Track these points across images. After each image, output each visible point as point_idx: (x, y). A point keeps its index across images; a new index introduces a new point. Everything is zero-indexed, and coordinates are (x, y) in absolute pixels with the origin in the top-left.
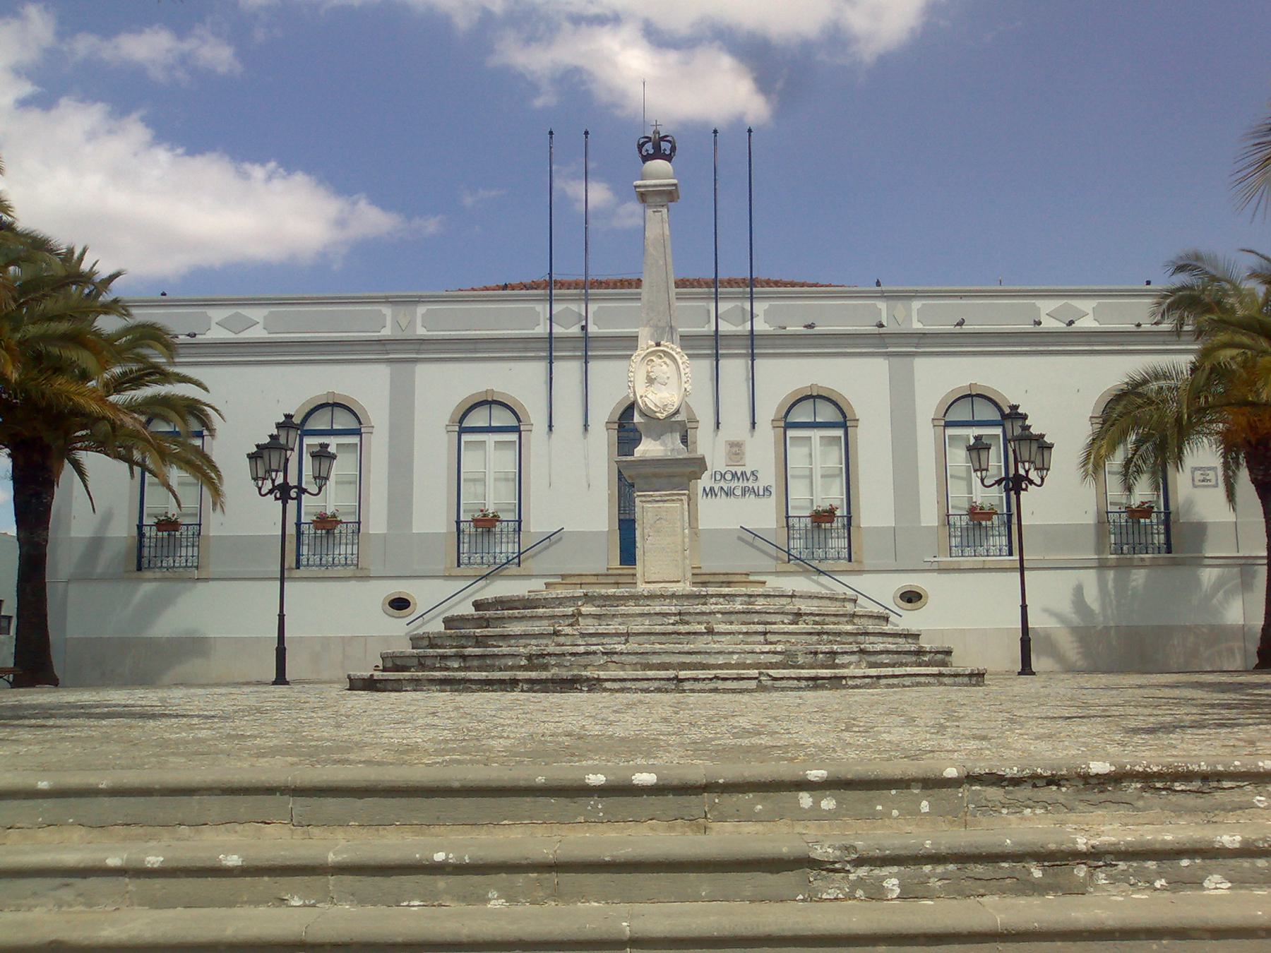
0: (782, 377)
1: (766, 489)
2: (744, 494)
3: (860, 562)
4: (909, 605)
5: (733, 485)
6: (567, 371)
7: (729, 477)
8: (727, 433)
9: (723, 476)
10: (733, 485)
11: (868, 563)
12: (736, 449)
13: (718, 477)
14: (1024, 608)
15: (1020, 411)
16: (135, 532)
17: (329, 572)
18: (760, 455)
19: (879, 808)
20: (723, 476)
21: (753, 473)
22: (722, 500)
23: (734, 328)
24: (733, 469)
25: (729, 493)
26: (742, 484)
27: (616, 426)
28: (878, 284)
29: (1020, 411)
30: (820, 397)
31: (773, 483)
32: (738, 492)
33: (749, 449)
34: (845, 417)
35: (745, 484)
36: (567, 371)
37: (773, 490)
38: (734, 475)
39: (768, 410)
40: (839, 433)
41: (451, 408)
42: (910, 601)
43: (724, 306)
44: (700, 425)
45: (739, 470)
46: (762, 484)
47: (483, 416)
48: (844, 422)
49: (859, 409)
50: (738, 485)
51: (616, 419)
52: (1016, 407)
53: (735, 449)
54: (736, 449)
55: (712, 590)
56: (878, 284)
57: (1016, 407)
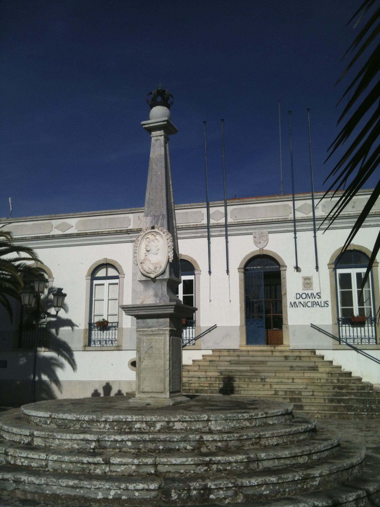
1: (326, 303)
2: (313, 306)
5: (306, 300)
6: (218, 242)
7: (304, 296)
9: (301, 296)
10: (306, 300)
12: (307, 282)
13: (298, 296)
14: (326, 161)
17: (104, 346)
20: (301, 296)
21: (317, 294)
23: (305, 216)
24: (306, 292)
25: (305, 305)
26: (311, 300)
27: (243, 270)
28: (236, 217)
31: (329, 300)
32: (309, 304)
33: (315, 282)
35: (314, 300)
36: (218, 242)
37: (330, 303)
38: (307, 295)
39: (326, 258)
43: (298, 204)
44: (288, 269)
45: (309, 292)
46: (324, 299)
51: (243, 267)
53: (307, 281)
54: (307, 282)
56: (236, 217)
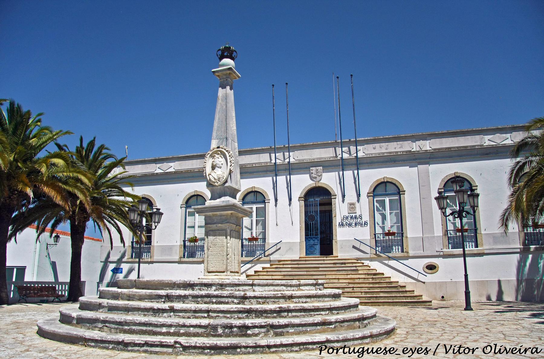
0: (370, 177)
3: (407, 252)
4: (430, 271)
8: (347, 200)
11: (411, 253)
14: (466, 276)
15: (160, 211)
16: (182, 243)
18: (364, 208)
19: (536, 293)
22: (346, 228)
25: (350, 225)
29: (160, 211)
30: (388, 182)
34: (399, 189)
38: (351, 217)
39: (365, 189)
40: (397, 198)
41: (506, 176)
42: (431, 269)
47: (385, 189)
48: (399, 192)
49: (405, 187)
50: (353, 222)
52: (159, 209)
53: (352, 206)
54: (352, 206)
55: (302, 282)
57: (159, 209)
